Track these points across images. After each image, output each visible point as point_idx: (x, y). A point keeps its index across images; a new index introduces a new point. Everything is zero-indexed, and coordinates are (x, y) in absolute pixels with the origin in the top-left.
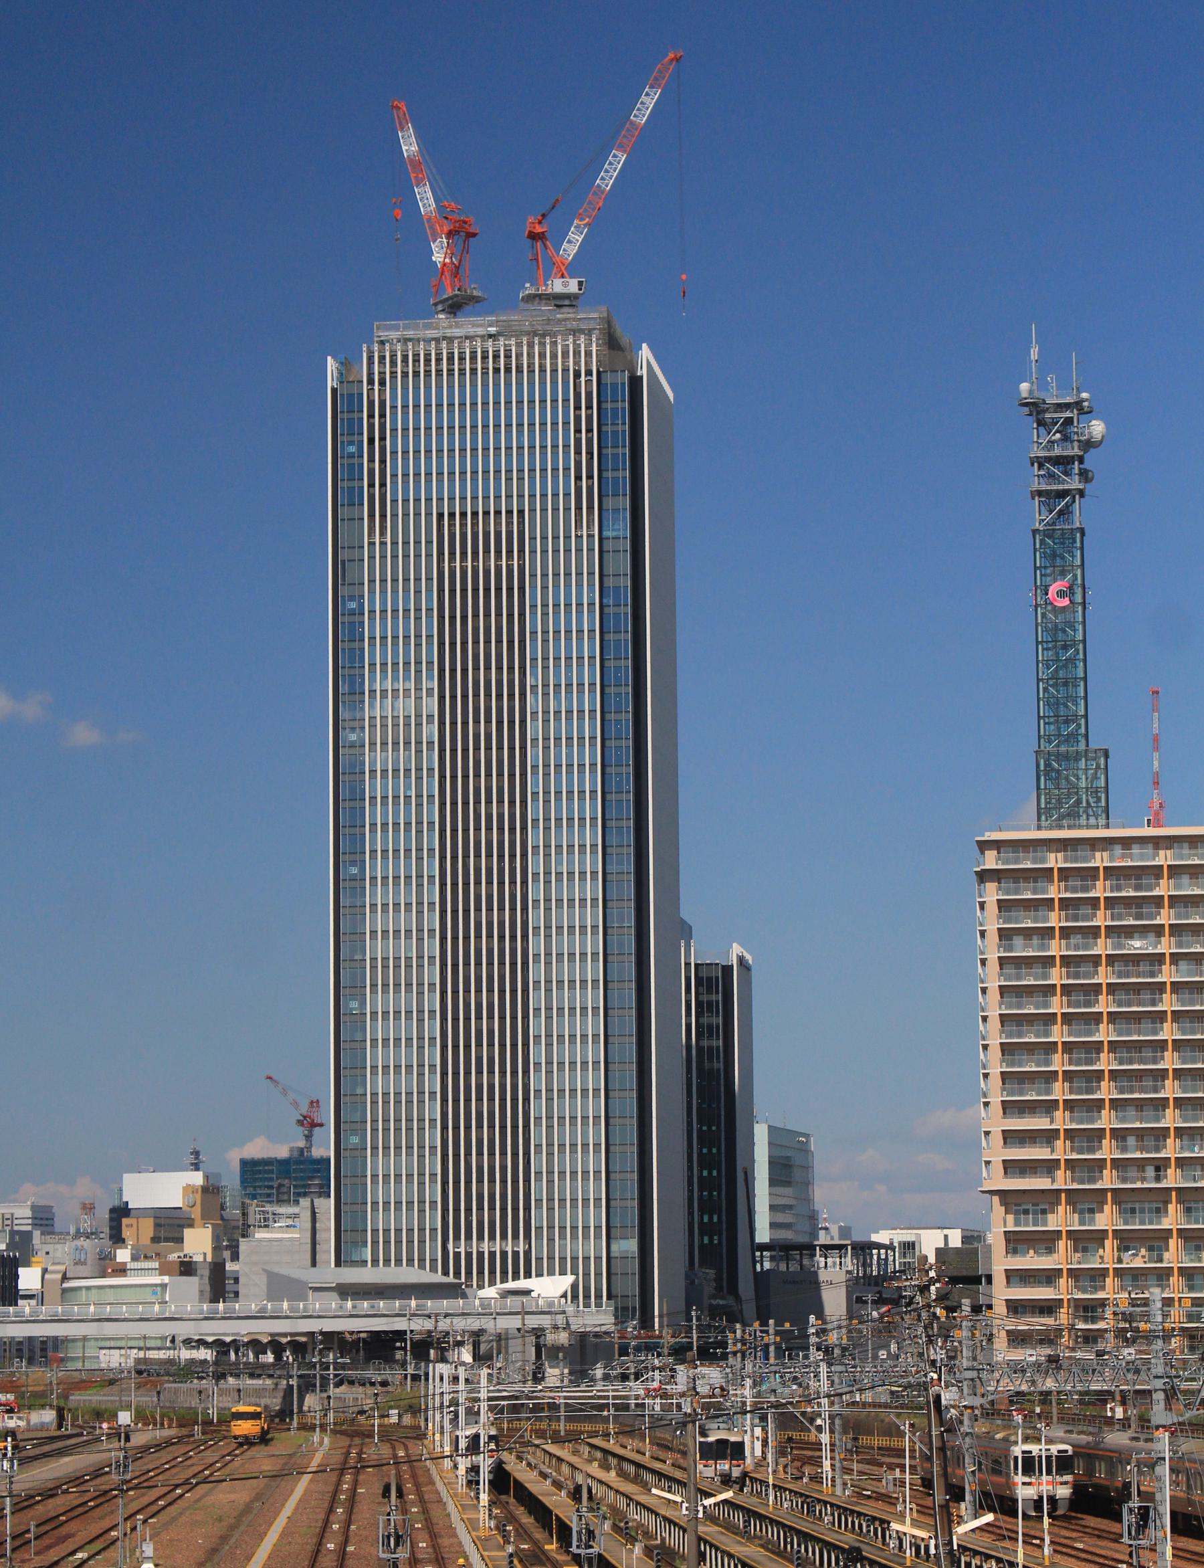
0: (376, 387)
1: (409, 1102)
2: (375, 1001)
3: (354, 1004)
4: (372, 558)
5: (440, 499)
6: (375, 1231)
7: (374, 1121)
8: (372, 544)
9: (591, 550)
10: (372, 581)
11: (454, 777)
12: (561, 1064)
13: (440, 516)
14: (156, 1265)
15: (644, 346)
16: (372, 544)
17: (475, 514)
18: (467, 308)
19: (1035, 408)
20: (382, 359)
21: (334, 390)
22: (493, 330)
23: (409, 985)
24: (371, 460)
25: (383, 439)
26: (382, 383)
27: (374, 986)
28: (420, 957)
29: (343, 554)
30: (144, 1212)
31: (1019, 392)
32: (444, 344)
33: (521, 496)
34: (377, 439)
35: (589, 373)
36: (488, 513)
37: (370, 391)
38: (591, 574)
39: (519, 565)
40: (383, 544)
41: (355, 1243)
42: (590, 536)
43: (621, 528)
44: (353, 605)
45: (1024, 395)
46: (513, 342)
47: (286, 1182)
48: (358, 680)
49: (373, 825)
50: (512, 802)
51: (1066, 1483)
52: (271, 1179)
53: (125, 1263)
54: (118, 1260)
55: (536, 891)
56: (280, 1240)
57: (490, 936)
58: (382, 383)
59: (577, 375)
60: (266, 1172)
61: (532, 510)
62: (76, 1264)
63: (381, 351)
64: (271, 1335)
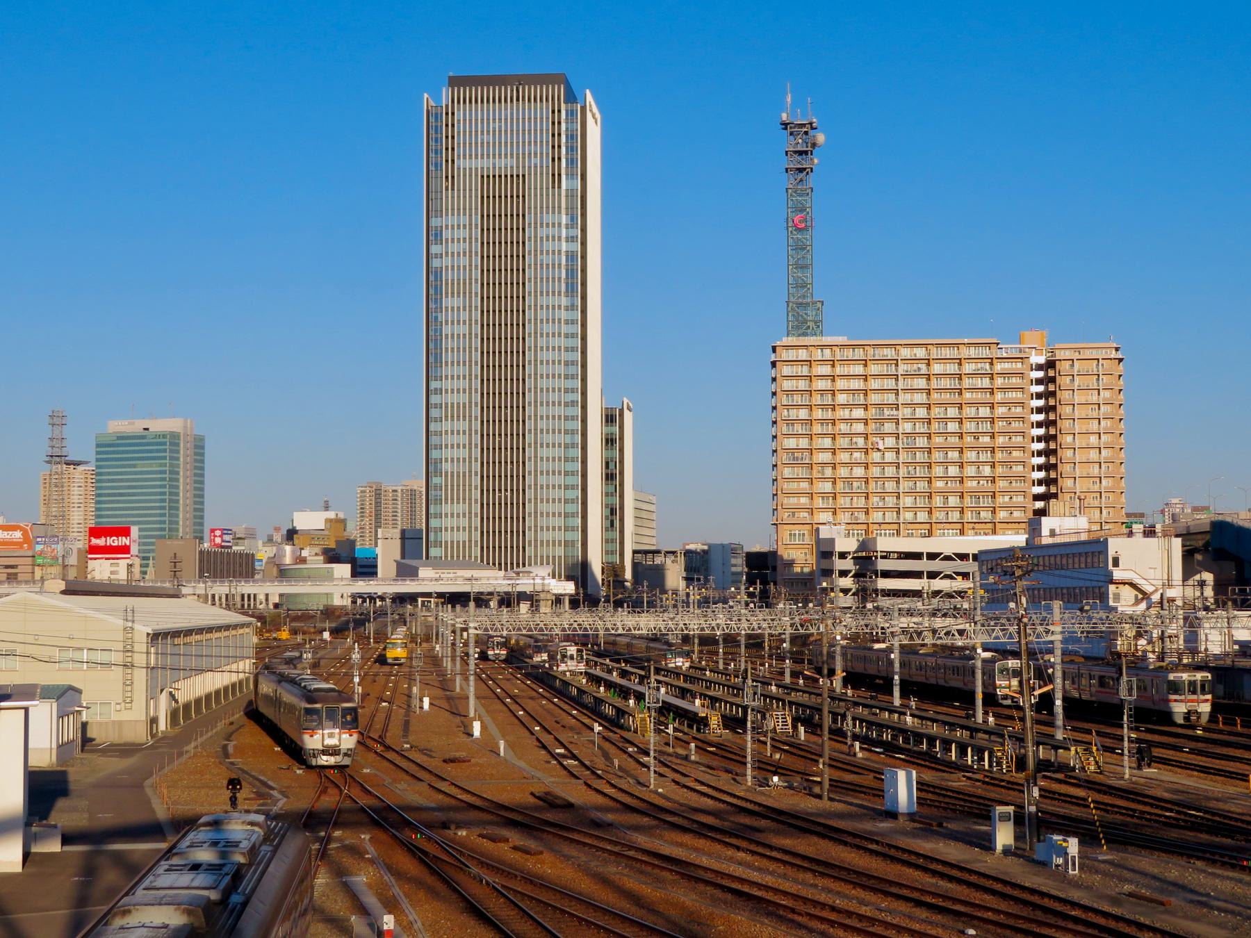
2: (448, 302)
13: (482, 177)
15: (588, 92)
19: (785, 125)
33: (524, 167)
51: (1207, 701)
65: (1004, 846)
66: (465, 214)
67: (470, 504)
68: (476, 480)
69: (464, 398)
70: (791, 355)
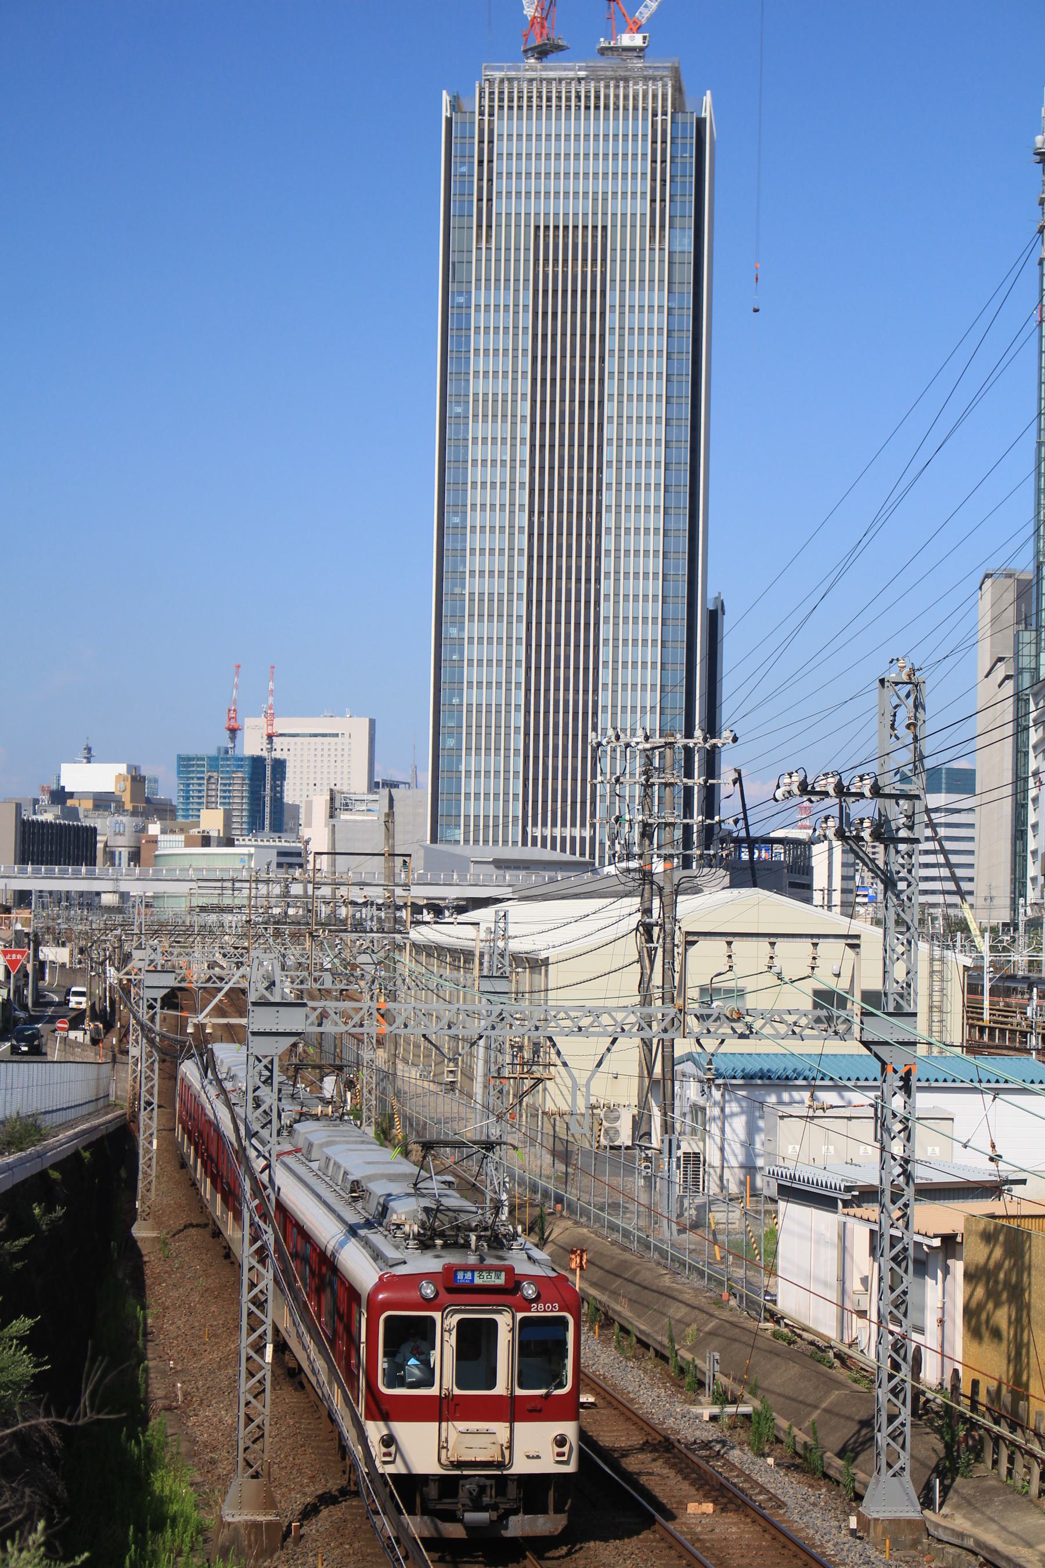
0: (486, 118)
1: (505, 401)
3: (454, 632)
4: (479, 260)
5: (537, 214)
6: (467, 816)
7: (469, 726)
8: (479, 249)
9: (661, 261)
10: (478, 280)
11: (542, 446)
12: (625, 685)
13: (537, 228)
14: (182, 837)
15: (708, 92)
16: (479, 249)
17: (566, 228)
18: (551, 56)
20: (626, 97)
21: (449, 121)
22: (582, 74)
23: (500, 616)
24: (480, 179)
25: (490, 161)
26: (491, 115)
27: (471, 615)
28: (511, 593)
29: (453, 256)
30: (84, 795)
31: (1034, 143)
32: (525, 85)
33: (605, 214)
35: (665, 113)
36: (596, 227)
37: (481, 121)
38: (661, 281)
39: (601, 272)
40: (488, 249)
41: (448, 826)
42: (662, 249)
43: (687, 243)
44: (461, 300)
45: (1039, 145)
46: (602, 84)
47: (215, 774)
48: (462, 451)
49: (477, 328)
50: (590, 469)
52: (203, 772)
53: (157, 836)
54: (150, 833)
55: (608, 542)
56: (363, 821)
57: (569, 578)
58: (491, 115)
59: (655, 115)
60: (198, 766)
61: (614, 226)
62: (116, 834)
63: (511, 88)
64: (428, 899)
65: (94, 830)
66: (507, 288)
67: (507, 757)
68: (515, 785)
69: (499, 586)
70: (486, 964)
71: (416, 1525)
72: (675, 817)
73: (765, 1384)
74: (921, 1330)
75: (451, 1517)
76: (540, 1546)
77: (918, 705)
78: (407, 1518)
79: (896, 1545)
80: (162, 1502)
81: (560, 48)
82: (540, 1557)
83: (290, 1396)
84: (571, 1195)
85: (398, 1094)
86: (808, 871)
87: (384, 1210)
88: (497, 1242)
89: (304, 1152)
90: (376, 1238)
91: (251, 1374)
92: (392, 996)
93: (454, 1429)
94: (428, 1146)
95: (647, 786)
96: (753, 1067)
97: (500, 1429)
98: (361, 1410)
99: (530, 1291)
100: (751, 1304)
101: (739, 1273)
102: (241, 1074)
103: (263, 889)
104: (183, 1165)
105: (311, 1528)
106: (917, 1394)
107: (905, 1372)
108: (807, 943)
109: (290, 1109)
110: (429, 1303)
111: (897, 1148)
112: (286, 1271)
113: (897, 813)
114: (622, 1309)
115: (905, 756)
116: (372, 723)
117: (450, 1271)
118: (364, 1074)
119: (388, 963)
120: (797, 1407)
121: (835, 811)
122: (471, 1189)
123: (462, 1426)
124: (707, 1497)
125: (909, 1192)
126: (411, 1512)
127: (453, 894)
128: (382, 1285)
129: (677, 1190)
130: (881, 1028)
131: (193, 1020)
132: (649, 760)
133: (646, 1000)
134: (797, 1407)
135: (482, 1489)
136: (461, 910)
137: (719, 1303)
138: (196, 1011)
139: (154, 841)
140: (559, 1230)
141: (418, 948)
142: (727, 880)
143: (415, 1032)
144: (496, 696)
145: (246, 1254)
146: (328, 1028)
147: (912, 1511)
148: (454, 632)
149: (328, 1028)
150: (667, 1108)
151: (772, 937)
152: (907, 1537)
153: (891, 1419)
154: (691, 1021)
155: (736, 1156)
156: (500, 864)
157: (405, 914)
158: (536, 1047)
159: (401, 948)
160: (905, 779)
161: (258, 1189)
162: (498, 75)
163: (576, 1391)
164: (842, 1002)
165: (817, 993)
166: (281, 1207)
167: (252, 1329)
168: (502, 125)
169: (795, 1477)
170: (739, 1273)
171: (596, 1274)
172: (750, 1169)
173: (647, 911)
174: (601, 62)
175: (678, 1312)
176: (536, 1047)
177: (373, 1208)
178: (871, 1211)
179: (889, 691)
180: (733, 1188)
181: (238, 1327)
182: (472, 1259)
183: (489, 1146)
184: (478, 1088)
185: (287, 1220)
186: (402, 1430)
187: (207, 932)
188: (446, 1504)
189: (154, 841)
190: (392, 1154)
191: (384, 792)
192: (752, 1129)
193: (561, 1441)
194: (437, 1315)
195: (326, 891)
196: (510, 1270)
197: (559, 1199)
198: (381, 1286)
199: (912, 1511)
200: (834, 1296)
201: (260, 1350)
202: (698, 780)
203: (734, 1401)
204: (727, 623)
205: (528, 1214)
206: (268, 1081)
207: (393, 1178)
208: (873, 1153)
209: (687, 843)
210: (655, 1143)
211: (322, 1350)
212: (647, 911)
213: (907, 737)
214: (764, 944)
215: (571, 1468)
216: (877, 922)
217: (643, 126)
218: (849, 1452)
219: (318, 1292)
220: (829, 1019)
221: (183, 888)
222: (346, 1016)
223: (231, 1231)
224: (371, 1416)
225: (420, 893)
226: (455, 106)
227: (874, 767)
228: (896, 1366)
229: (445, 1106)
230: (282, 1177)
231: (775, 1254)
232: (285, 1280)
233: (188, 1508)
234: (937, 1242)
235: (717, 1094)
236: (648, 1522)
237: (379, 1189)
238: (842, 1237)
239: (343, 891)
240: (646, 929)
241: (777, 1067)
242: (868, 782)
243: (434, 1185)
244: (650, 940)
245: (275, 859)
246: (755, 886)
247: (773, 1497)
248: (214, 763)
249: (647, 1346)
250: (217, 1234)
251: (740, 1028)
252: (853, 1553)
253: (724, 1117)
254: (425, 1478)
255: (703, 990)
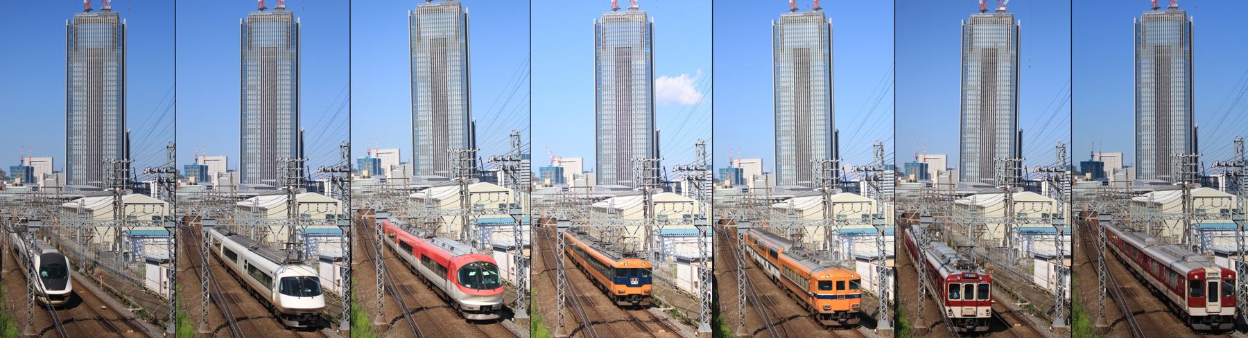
21: (68, 26)
34: (1144, 32)
69: (255, 127)
71: (956, 329)
72: (1012, 176)
73: (1032, 298)
74: (1065, 287)
75: (964, 327)
76: (983, 333)
77: (882, 150)
78: (954, 327)
79: (1060, 333)
80: (902, 324)
81: (266, 8)
82: (983, 335)
83: (928, 301)
84: (990, 258)
85: (952, 236)
86: (1041, 188)
87: (949, 261)
88: (974, 268)
89: (932, 248)
90: (948, 267)
91: (30, 302)
92: (951, 215)
93: (964, 308)
94: (959, 247)
95: (823, 171)
96: (1029, 230)
97: (974, 308)
98: (944, 304)
99: (981, 278)
100: (1029, 281)
101: (1026, 274)
102: (918, 231)
103: (559, 196)
104: (906, 251)
105: (933, 329)
106: (1064, 300)
107: (1062, 296)
108: (152, 205)
109: (929, 239)
110: (959, 281)
111: (882, 248)
112: (928, 274)
113: (1060, 175)
114: (1001, 282)
115: (880, 161)
116: (1122, 154)
117: (964, 274)
118: (945, 232)
119: (950, 208)
120: (151, 309)
121: (1047, 175)
122: (968, 256)
123: (966, 307)
124: (1019, 323)
125: (885, 258)
126: (955, 326)
127: (964, 193)
128: (949, 277)
129: (1013, 256)
130: (877, 222)
131: (1086, 218)
132: (1006, 164)
133: (1006, 216)
134: (1038, 303)
135: (970, 321)
136: (783, 200)
137: (1022, 281)
138: (909, 218)
139: (5, 185)
140: (987, 265)
141: (956, 204)
142: (663, 191)
143: (956, 222)
144: (973, 150)
145: (919, 270)
146: (937, 222)
147: (1063, 326)
148: (71, 138)
149: (937, 222)
150: (1010, 239)
151: (144, 204)
152: (1062, 331)
153: (1059, 306)
154: (835, 222)
155: (846, 251)
156: (1151, 184)
157: (954, 197)
158: (982, 226)
159: (953, 204)
160: (1062, 168)
161: (922, 256)
162: (784, 16)
163: (991, 300)
164: (1048, 216)
165: (1043, 214)
166: (927, 260)
167: (204, 291)
168: (975, 27)
169: (1038, 318)
170: (1026, 274)
171: (995, 275)
172: (1028, 252)
173: (289, 197)
174: (101, 12)
175: (1013, 283)
176: (982, 226)
177: (947, 261)
178: (1054, 261)
179: (698, 146)
180: (846, 258)
181: (201, 290)
182: (968, 271)
183: (972, 247)
184: (78, 239)
185: (928, 263)
186: (953, 308)
187: (17, 205)
188: (962, 325)
189: (899, 181)
190: (951, 249)
191: (230, 172)
192: (1029, 244)
193: (987, 311)
194: (961, 284)
195: (43, 196)
196: (976, 274)
197: (987, 259)
198: (949, 277)
199: (1063, 326)
200: (869, 280)
201: (1103, 290)
202: (1017, 168)
203: (1025, 302)
204: (1023, 134)
205: (980, 262)
206: (924, 233)
207: (951, 254)
208: (1055, 248)
209: (1015, 182)
210: (118, 250)
211: (936, 292)
212: (1006, 196)
213: (1062, 159)
214: (850, 204)
215: (989, 317)
216: (1056, 199)
217: (1005, 27)
218: (1049, 313)
219: (935, 278)
220: (1045, 220)
221: (186, 194)
222: (758, 223)
223: (916, 265)
224: (946, 305)
225: (774, 197)
226: (965, 23)
227: (340, 165)
228: (1060, 295)
229: (963, 238)
230: (927, 254)
231: (145, 274)
232: (928, 276)
233: (907, 325)
234: (891, 269)
235: (1021, 236)
236: (1006, 328)
237: (948, 256)
238: (1048, 267)
239: (757, 197)
240: (115, 203)
241: (1034, 230)
242: (694, 167)
243: (960, 255)
244: (646, 204)
245: (562, 189)
246: (848, 192)
247: (146, 329)
248: (18, 168)
249: (117, 296)
250: (913, 266)
251: (311, 223)
252: (1051, 335)
253: (1023, 241)
254: (958, 319)
255: (1018, 214)
